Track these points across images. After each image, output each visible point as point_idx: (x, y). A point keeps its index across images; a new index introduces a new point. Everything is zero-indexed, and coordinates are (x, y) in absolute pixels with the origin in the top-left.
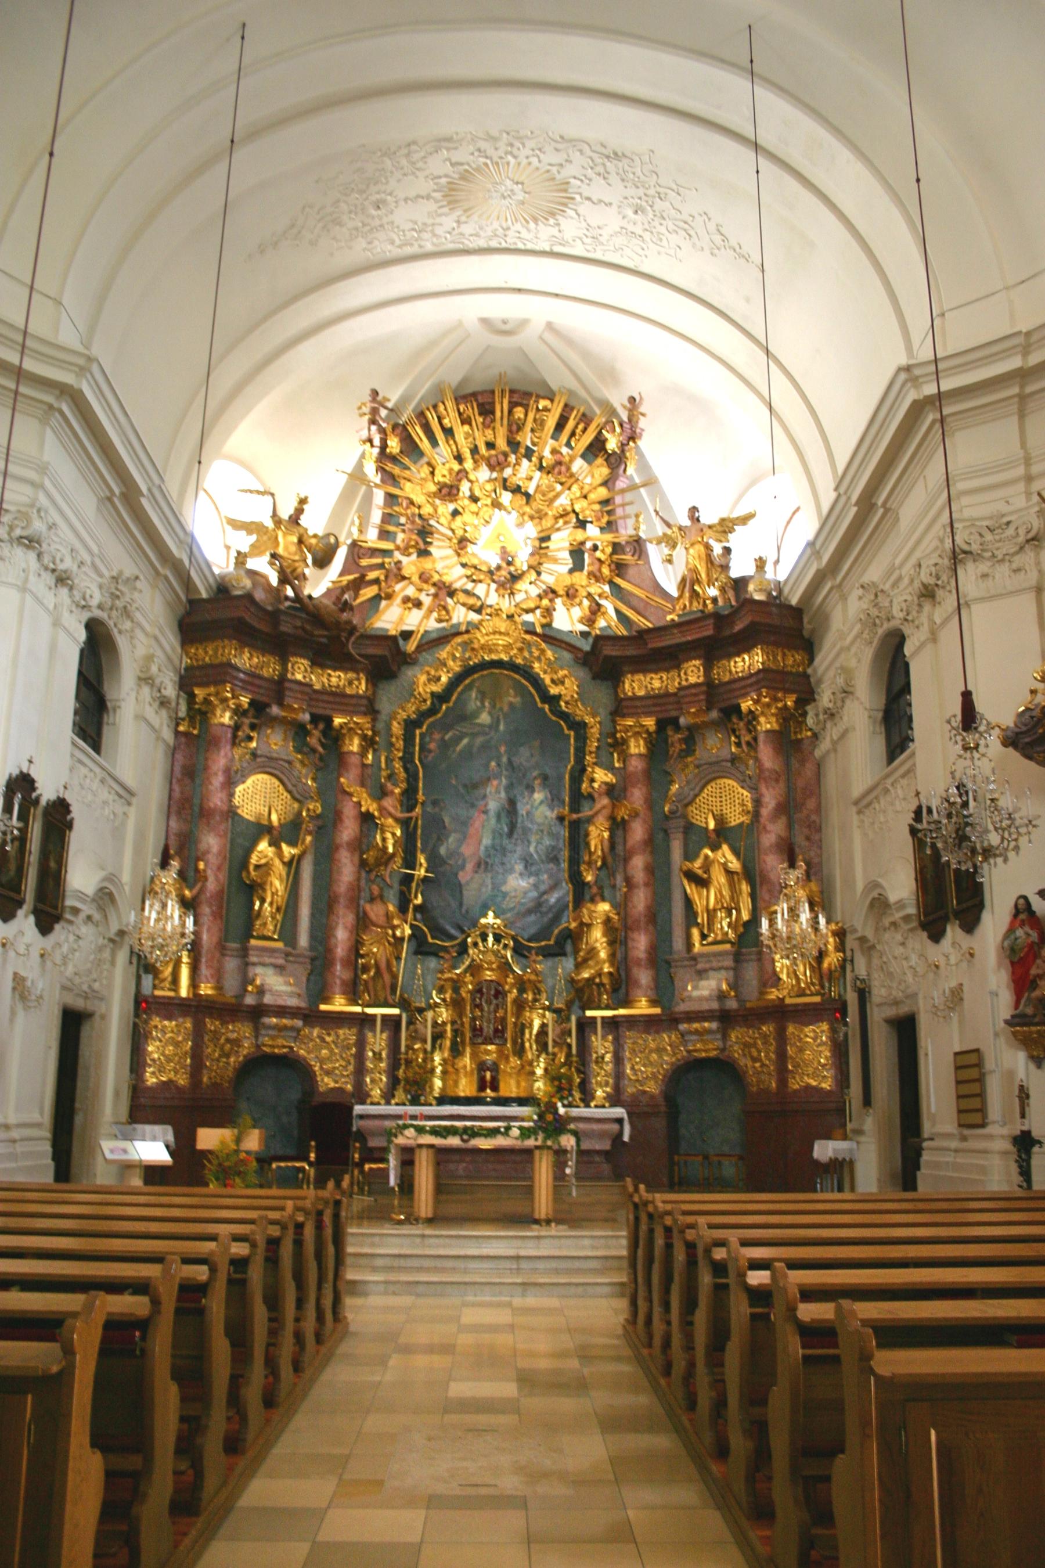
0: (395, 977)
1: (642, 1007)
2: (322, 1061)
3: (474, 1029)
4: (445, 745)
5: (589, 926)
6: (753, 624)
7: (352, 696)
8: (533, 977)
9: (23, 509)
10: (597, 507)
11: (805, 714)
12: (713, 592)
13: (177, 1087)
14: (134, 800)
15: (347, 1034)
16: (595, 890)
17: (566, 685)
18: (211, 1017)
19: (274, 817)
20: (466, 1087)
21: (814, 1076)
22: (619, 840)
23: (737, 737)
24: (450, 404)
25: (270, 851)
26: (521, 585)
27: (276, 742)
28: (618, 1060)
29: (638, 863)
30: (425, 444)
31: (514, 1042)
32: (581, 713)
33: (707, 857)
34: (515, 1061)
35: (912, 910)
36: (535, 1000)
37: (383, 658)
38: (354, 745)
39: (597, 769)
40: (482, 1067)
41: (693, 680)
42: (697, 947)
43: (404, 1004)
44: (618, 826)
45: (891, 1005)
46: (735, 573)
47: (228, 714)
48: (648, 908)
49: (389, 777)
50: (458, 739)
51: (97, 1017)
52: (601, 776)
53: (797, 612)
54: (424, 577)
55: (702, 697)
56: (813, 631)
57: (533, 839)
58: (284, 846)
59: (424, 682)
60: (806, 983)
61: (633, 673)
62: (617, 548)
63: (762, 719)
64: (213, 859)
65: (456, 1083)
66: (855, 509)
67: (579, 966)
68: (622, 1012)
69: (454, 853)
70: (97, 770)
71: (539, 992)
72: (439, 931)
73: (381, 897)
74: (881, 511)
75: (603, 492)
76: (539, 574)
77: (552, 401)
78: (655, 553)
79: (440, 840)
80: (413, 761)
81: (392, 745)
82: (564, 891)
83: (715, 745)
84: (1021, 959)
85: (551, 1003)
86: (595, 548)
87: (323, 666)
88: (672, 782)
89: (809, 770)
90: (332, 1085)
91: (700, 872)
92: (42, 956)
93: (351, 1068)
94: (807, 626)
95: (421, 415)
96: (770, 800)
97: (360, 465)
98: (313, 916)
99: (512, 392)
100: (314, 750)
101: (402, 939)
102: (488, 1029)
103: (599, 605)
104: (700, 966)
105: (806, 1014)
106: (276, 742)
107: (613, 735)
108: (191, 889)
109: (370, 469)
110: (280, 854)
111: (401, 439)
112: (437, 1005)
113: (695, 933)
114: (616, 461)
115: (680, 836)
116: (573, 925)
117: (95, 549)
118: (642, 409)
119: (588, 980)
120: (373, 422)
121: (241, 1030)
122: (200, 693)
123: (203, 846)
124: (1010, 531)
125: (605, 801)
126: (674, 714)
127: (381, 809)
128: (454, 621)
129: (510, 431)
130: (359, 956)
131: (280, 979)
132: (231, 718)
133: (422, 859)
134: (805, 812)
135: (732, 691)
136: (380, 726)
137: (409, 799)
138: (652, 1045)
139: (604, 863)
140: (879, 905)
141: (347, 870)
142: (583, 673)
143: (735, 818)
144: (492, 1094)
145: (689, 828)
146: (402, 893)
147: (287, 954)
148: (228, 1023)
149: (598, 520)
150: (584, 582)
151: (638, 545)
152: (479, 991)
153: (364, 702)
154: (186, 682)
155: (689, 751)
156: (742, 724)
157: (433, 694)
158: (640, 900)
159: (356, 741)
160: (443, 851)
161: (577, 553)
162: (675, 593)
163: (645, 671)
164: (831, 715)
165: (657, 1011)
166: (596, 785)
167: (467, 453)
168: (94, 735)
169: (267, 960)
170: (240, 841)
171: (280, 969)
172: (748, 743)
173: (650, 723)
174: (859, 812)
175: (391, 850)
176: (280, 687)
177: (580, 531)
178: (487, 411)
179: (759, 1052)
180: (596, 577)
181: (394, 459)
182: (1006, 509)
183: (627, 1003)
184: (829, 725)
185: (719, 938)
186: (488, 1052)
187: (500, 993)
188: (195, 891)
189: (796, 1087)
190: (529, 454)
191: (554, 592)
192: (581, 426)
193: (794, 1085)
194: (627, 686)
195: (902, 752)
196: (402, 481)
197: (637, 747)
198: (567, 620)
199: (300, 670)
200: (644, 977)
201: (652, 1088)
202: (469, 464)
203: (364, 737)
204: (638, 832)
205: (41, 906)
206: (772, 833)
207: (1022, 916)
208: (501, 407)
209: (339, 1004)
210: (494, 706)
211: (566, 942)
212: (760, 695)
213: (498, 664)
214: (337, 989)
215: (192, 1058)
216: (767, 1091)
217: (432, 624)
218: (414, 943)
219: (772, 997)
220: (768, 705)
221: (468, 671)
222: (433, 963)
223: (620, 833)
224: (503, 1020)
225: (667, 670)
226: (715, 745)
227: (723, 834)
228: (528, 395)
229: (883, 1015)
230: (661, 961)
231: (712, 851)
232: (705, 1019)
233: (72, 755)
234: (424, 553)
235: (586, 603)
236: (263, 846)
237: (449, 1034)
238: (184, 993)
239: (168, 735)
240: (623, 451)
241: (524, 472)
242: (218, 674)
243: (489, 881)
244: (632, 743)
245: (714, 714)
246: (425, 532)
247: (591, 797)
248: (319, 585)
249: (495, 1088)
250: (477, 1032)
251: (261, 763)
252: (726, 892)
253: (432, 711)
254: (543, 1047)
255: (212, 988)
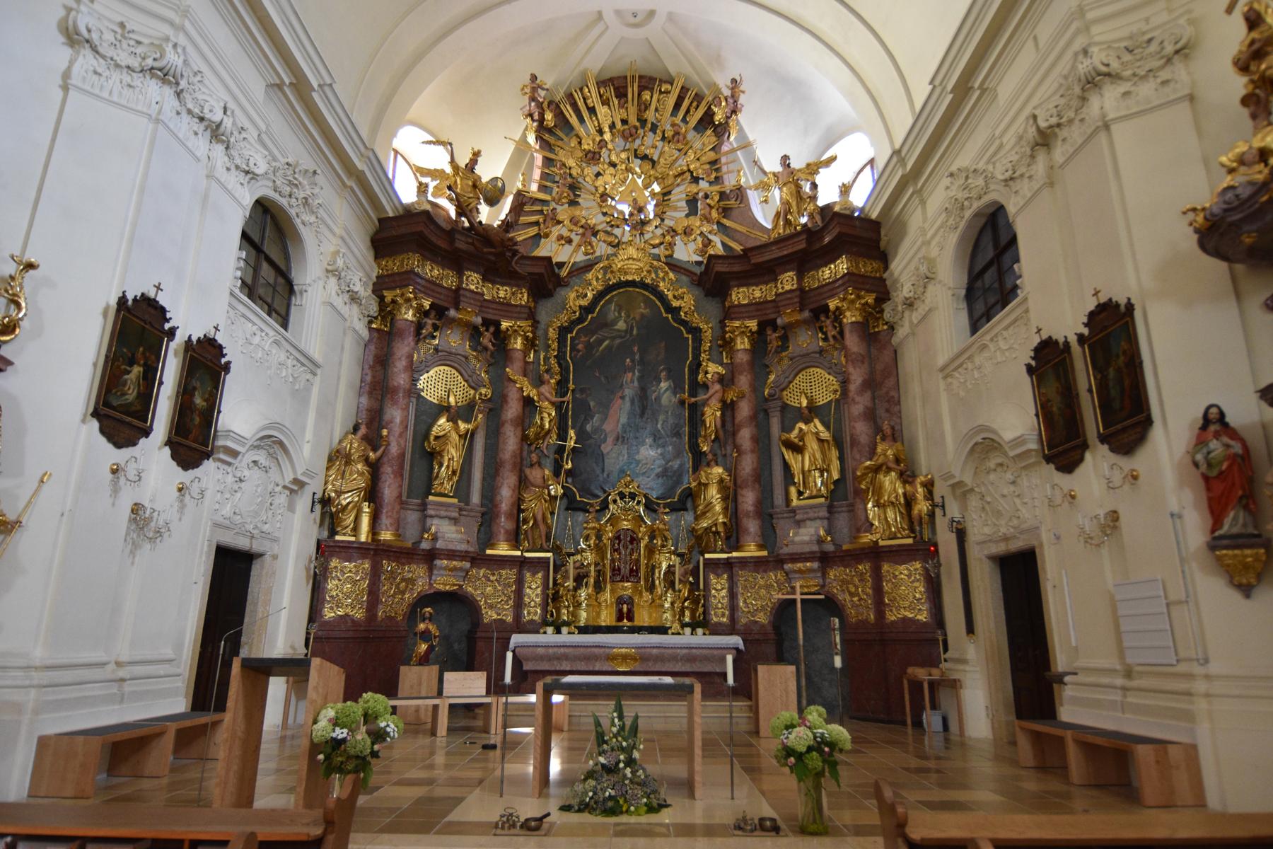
0: (549, 528)
1: (751, 551)
2: (486, 597)
3: (613, 570)
4: (589, 347)
5: (706, 485)
6: (840, 235)
7: (516, 306)
8: (661, 526)
9: (156, 42)
10: (708, 166)
11: (882, 311)
12: (804, 220)
13: (353, 621)
14: (319, 371)
15: (509, 574)
16: (710, 457)
17: (686, 300)
18: (388, 558)
19: (452, 400)
20: (607, 618)
21: (910, 608)
22: (728, 419)
23: (824, 333)
24: (592, 88)
25: (448, 426)
26: (650, 228)
27: (454, 340)
28: (732, 595)
29: (745, 436)
30: (574, 120)
31: (646, 581)
32: (696, 320)
33: (801, 430)
34: (647, 596)
35: (1033, 446)
36: (663, 546)
37: (541, 275)
38: (518, 344)
39: (710, 364)
40: (620, 601)
41: (788, 287)
42: (795, 502)
43: (556, 550)
44: (728, 408)
45: (997, 542)
46: (821, 202)
47: (411, 313)
48: (754, 470)
49: (547, 371)
50: (600, 342)
51: (267, 558)
52: (713, 369)
53: (875, 225)
54: (574, 221)
55: (796, 300)
56: (888, 242)
57: (661, 417)
58: (460, 422)
59: (574, 298)
60: (897, 527)
61: (739, 286)
62: (723, 195)
63: (848, 314)
64: (397, 429)
65: (598, 614)
66: (951, 96)
67: (697, 518)
68: (735, 554)
69: (597, 430)
70: (272, 333)
71: (666, 540)
72: (586, 492)
73: (540, 465)
74: (977, 93)
75: (712, 156)
76: (663, 220)
77: (672, 84)
78: (754, 198)
79: (586, 420)
80: (565, 358)
81: (549, 346)
82: (688, 460)
83: (805, 340)
84: (1221, 473)
85: (676, 549)
86: (706, 196)
87: (493, 283)
88: (769, 373)
89: (887, 356)
90: (495, 616)
91: (796, 440)
92: (180, 490)
93: (511, 602)
94: (884, 239)
95: (570, 96)
96: (857, 377)
97: (524, 136)
98: (484, 479)
99: (640, 77)
100: (486, 349)
101: (555, 497)
102: (625, 570)
103: (710, 241)
104: (798, 517)
105: (900, 555)
106: (454, 340)
107: (723, 338)
108: (375, 450)
109: (531, 139)
110: (457, 428)
111: (553, 119)
112: (583, 550)
113: (793, 490)
114: (721, 131)
115: (778, 414)
116: (694, 484)
117: (263, 127)
118: (742, 88)
119: (706, 529)
120: (533, 99)
121: (418, 572)
122: (389, 298)
123: (387, 417)
124: (1153, 47)
125: (717, 387)
126: (773, 316)
127: (539, 394)
128: (598, 254)
129: (640, 110)
130: (520, 511)
131: (453, 528)
132: (414, 315)
133: (572, 433)
134: (885, 390)
135: (821, 294)
136: (540, 333)
137: (562, 387)
138: (762, 582)
139: (717, 438)
140: (985, 447)
141: (511, 442)
142: (698, 292)
143: (822, 398)
144: (629, 624)
145: (785, 407)
146: (556, 461)
147: (461, 510)
148: (404, 564)
149: (709, 176)
150: (698, 223)
151: (740, 193)
152: (618, 538)
153: (527, 310)
154: (379, 287)
155: (784, 347)
156: (828, 322)
157: (580, 307)
158: (748, 464)
159: (519, 341)
160: (588, 428)
161: (692, 202)
162: (769, 226)
163: (747, 285)
164: (910, 304)
165: (765, 553)
166: (709, 376)
167: (606, 129)
168: (283, 313)
169: (443, 513)
170: (424, 417)
171: (455, 521)
172: (834, 337)
173: (753, 325)
174: (945, 378)
175: (547, 426)
176: (456, 296)
177: (694, 185)
178: (621, 94)
179: (857, 588)
180: (706, 219)
181: (550, 131)
182: (1145, 28)
183: (737, 548)
184: (907, 314)
185: (815, 493)
186: (625, 589)
187: (634, 540)
188: (379, 453)
189: (893, 618)
190: (654, 128)
191: (674, 231)
192: (695, 104)
193: (891, 617)
194: (734, 297)
195: (988, 321)
196: (557, 149)
197: (742, 344)
198: (686, 252)
199: (473, 281)
200: (752, 526)
201: (762, 618)
202: (607, 136)
203: (526, 338)
204: (744, 410)
205: (176, 439)
206: (859, 404)
207: (1213, 428)
208: (632, 90)
209: (503, 550)
210: (628, 316)
211: (687, 500)
212: (847, 292)
213: (632, 283)
214: (502, 537)
215: (369, 595)
216: (864, 623)
217: (580, 257)
218: (565, 501)
219: (865, 540)
220: (852, 302)
221: (609, 289)
222: (581, 516)
223: (728, 413)
224: (638, 561)
225: (766, 283)
226: (805, 340)
227: (813, 411)
228: (652, 80)
229: (986, 552)
230: (766, 514)
231: (806, 424)
232: (806, 560)
233: (230, 305)
234: (573, 203)
235: (699, 239)
236: (442, 421)
237: (593, 574)
238: (363, 538)
239: (365, 334)
240: (727, 123)
241: (649, 143)
242: (405, 278)
243: (625, 452)
244: (739, 340)
245: (806, 314)
246: (574, 187)
247: (706, 387)
248: (487, 215)
249: (630, 619)
250: (616, 571)
251: (443, 357)
252: (818, 456)
253: (580, 320)
254: (671, 584)
255: (534, 574)
